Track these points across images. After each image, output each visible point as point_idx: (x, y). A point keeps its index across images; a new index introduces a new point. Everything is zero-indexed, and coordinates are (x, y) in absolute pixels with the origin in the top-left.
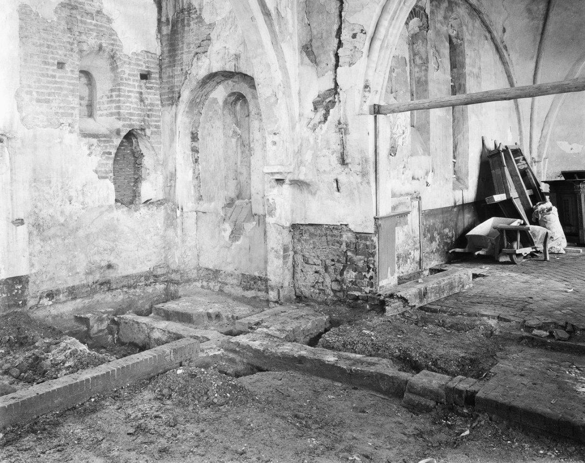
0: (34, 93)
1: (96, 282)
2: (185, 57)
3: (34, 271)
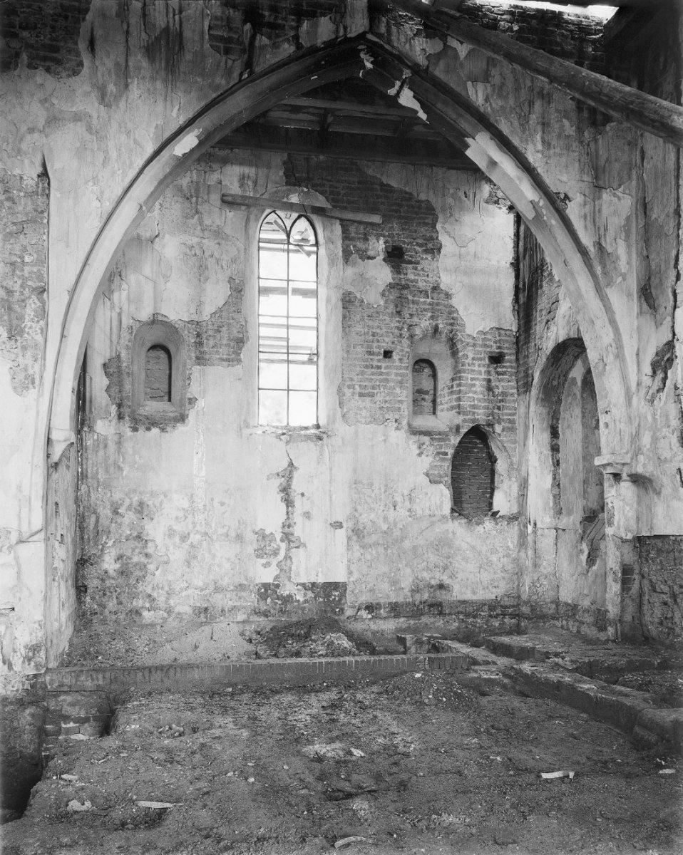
0: (357, 387)
1: (424, 602)
2: (538, 328)
3: (352, 579)
